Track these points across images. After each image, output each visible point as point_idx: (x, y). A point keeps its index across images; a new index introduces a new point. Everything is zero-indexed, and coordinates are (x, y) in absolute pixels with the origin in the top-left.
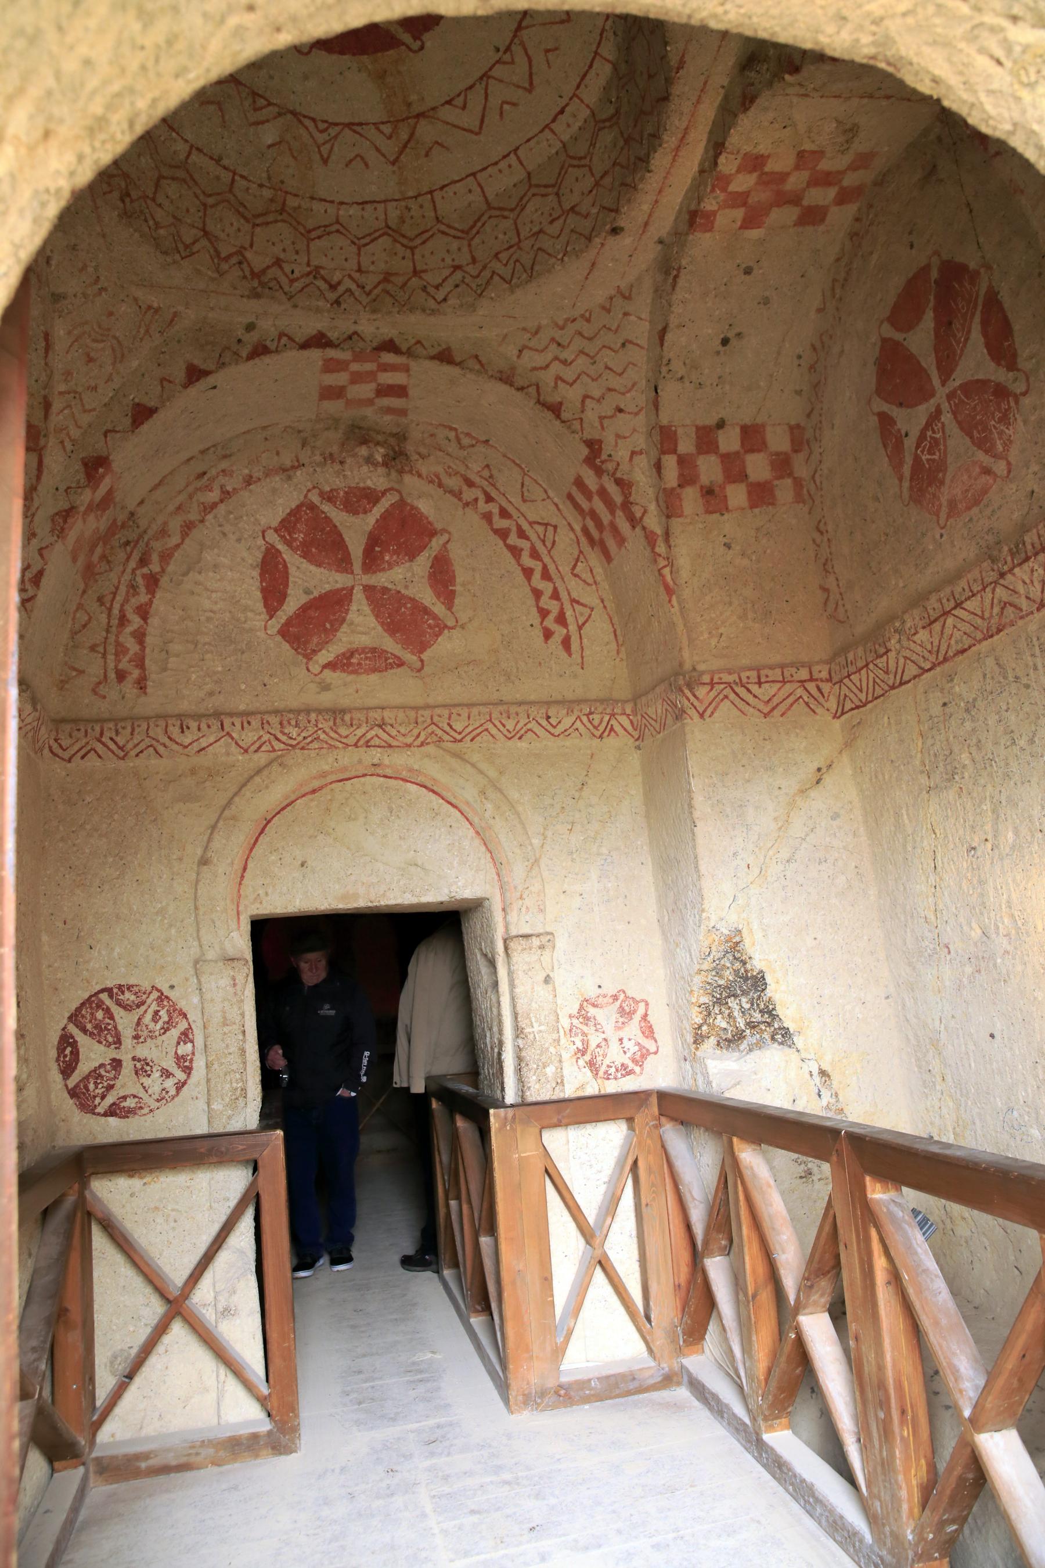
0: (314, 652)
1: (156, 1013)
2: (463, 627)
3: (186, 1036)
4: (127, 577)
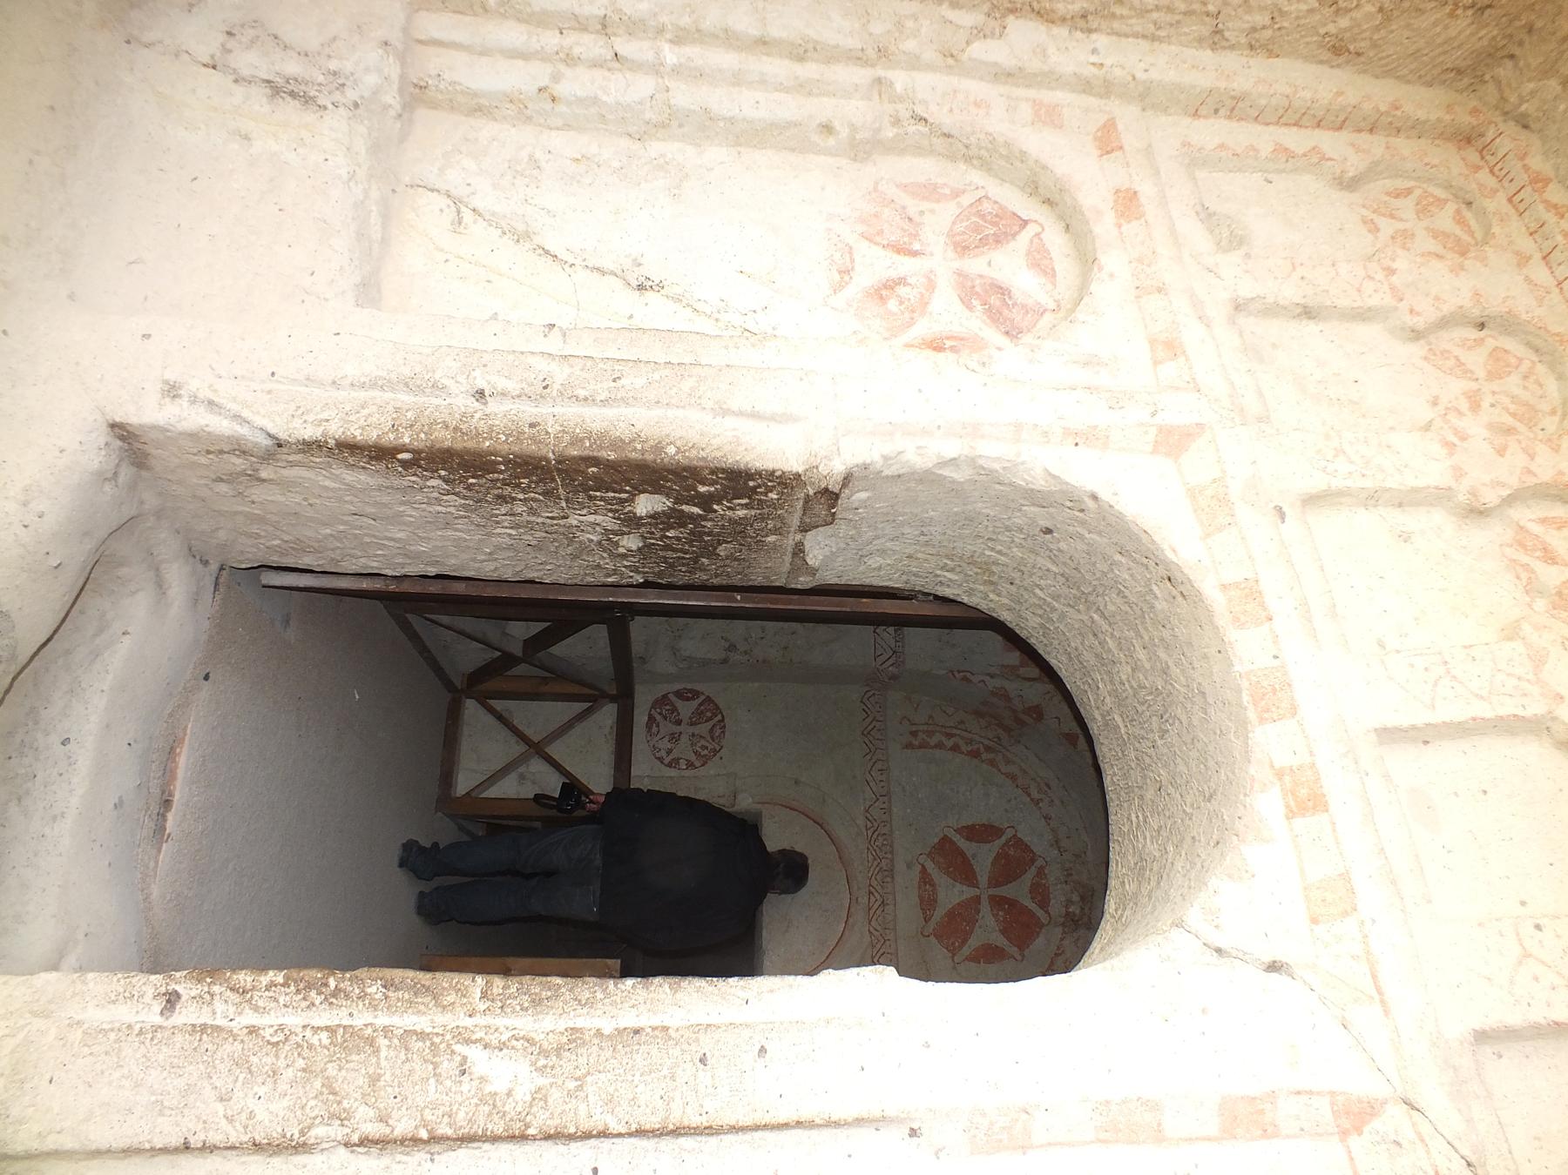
0: (933, 860)
1: (707, 748)
2: (954, 968)
3: (690, 765)
4: (977, 738)
